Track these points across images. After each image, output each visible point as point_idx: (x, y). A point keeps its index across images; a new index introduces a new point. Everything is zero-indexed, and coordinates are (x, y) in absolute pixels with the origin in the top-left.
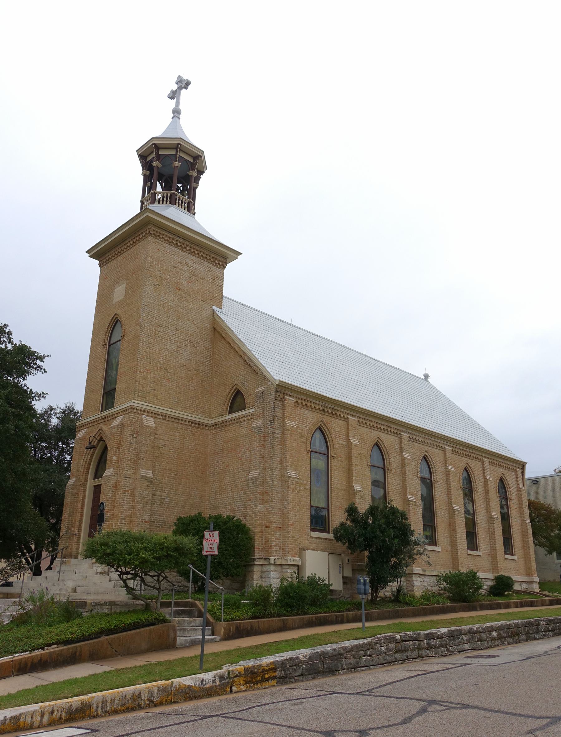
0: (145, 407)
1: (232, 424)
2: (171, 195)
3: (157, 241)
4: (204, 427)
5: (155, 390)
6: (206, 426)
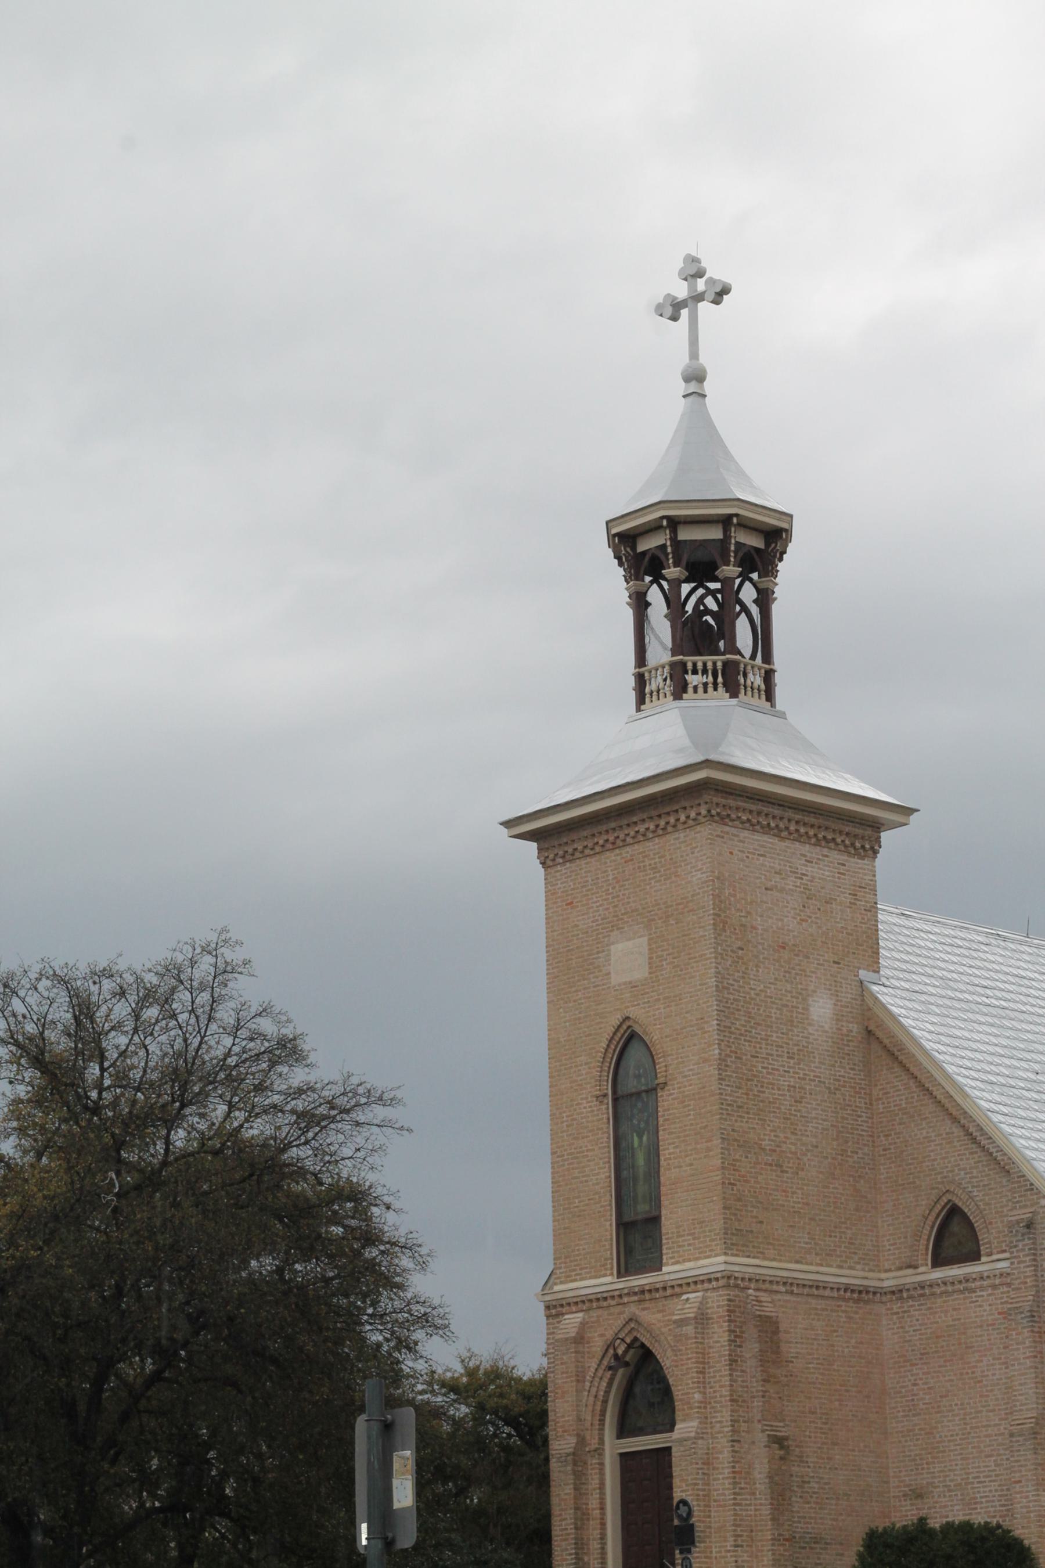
0: (750, 1270)
1: (946, 1292)
2: (725, 664)
3: (727, 829)
4: (871, 1296)
5: (761, 1222)
6: (875, 1293)
